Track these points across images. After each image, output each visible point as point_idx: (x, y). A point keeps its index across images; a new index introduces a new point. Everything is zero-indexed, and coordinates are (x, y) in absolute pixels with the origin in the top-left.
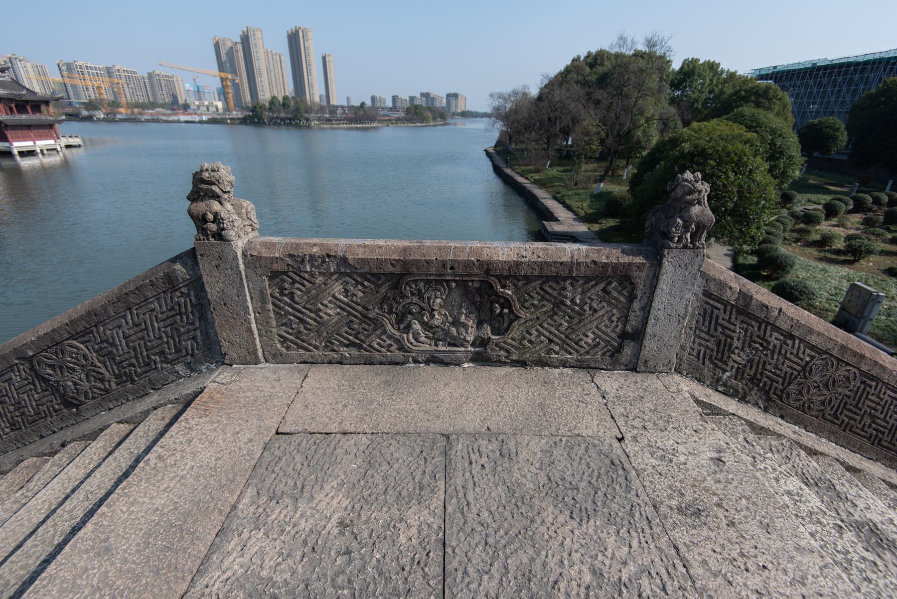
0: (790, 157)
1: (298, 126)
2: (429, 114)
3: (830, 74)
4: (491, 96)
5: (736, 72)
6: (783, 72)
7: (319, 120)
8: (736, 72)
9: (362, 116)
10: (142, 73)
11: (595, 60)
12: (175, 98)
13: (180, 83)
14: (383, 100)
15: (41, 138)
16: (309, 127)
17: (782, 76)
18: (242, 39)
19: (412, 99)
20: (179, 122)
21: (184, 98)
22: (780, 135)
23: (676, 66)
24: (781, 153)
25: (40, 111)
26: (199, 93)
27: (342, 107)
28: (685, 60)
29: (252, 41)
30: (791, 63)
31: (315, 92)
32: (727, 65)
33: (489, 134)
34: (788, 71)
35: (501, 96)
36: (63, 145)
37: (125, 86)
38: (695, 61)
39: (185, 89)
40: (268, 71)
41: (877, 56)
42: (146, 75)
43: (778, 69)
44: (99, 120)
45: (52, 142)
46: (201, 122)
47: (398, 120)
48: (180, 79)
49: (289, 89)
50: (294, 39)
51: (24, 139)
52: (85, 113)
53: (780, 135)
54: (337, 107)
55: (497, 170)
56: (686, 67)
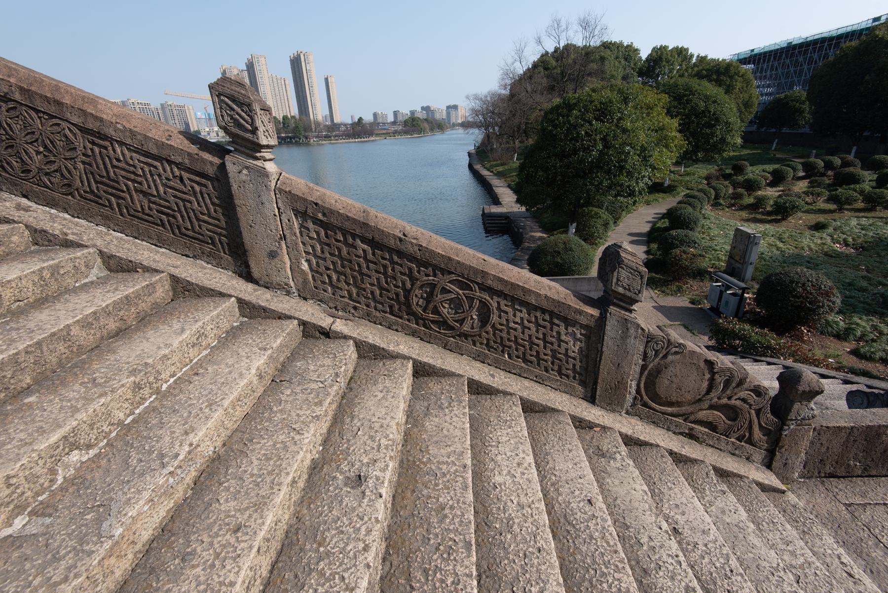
0: (727, 124)
1: (298, 144)
2: (426, 125)
3: (806, 52)
4: (467, 97)
5: (706, 57)
6: (760, 54)
7: (317, 137)
8: (706, 57)
9: (359, 130)
11: (563, 54)
13: (192, 111)
14: (385, 116)
16: (308, 144)
17: (759, 59)
18: (247, 66)
19: (412, 113)
22: (715, 102)
23: (644, 54)
24: (717, 120)
27: (345, 125)
28: (654, 48)
29: (257, 68)
30: (767, 44)
31: (319, 112)
32: (697, 49)
33: (473, 138)
34: (765, 53)
35: (476, 97)
38: (663, 49)
41: (849, 29)
42: (159, 107)
43: (756, 52)
47: (395, 133)
48: (191, 107)
49: (294, 111)
50: (296, 64)
53: (715, 102)
54: (340, 125)
55: (470, 166)
56: (654, 54)
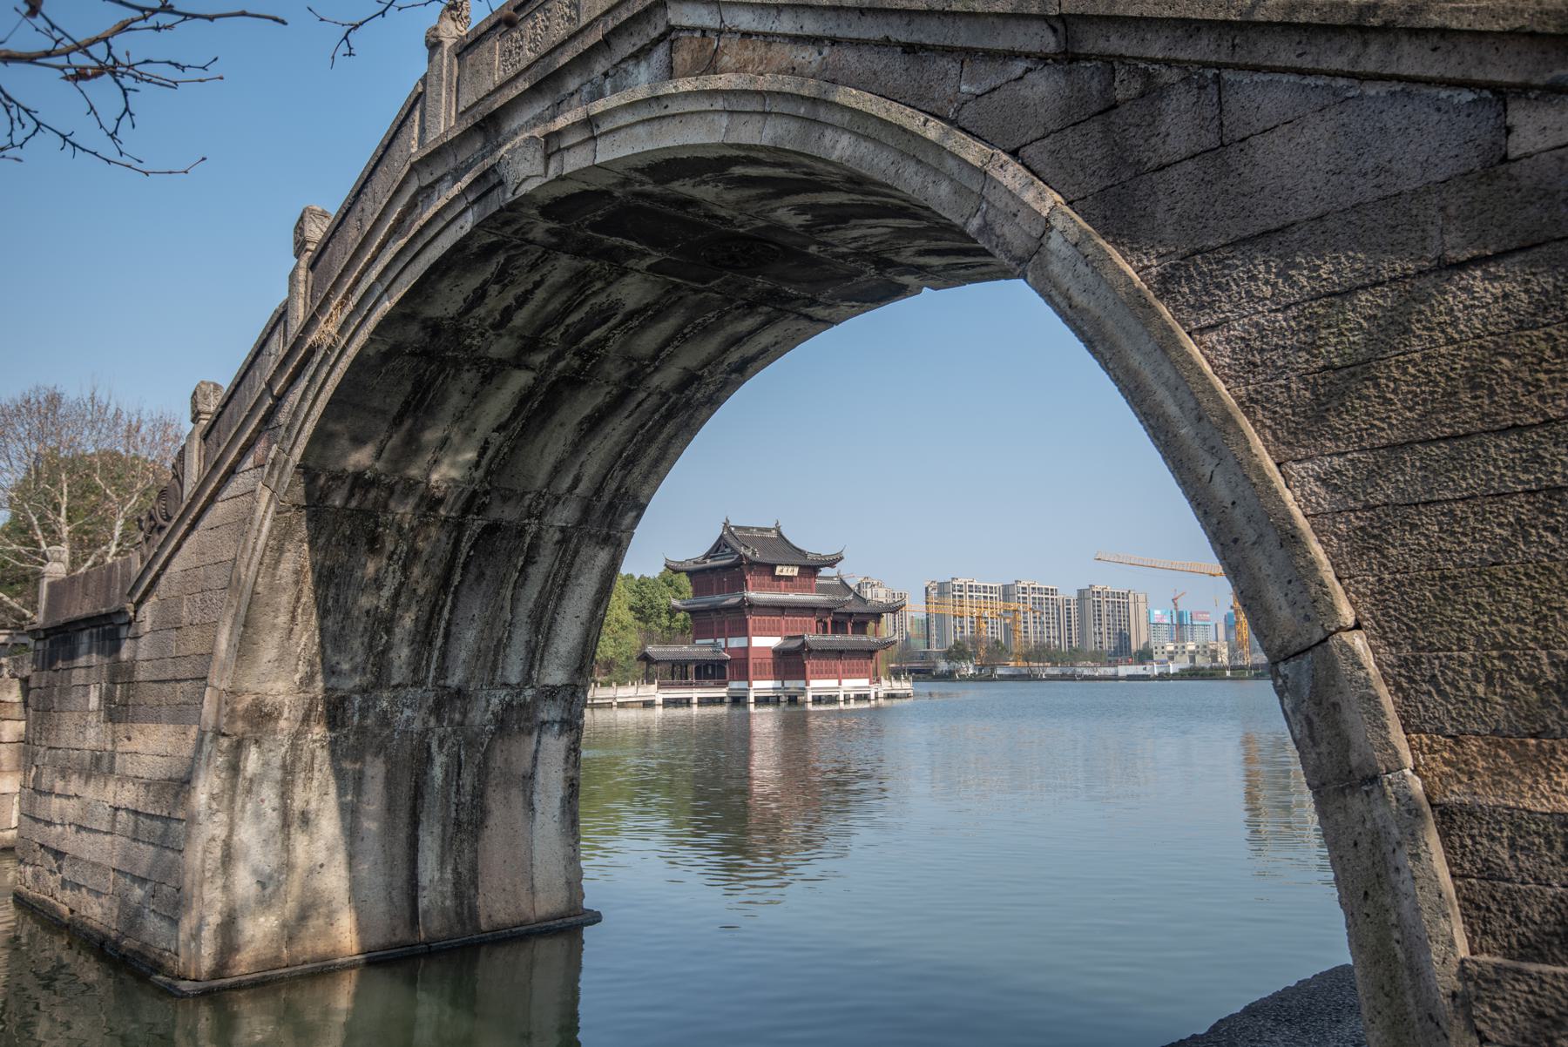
10: (1068, 592)
12: (1124, 638)
13: (1142, 606)
15: (851, 674)
20: (1116, 678)
21: (1143, 640)
25: (864, 633)
26: (1180, 627)
36: (881, 695)
37: (1030, 615)
39: (1150, 618)
40: (420, 232)
42: (1074, 596)
44: (963, 679)
45: (865, 682)
46: (1162, 677)
48: (1141, 598)
51: (827, 674)
52: (943, 666)
